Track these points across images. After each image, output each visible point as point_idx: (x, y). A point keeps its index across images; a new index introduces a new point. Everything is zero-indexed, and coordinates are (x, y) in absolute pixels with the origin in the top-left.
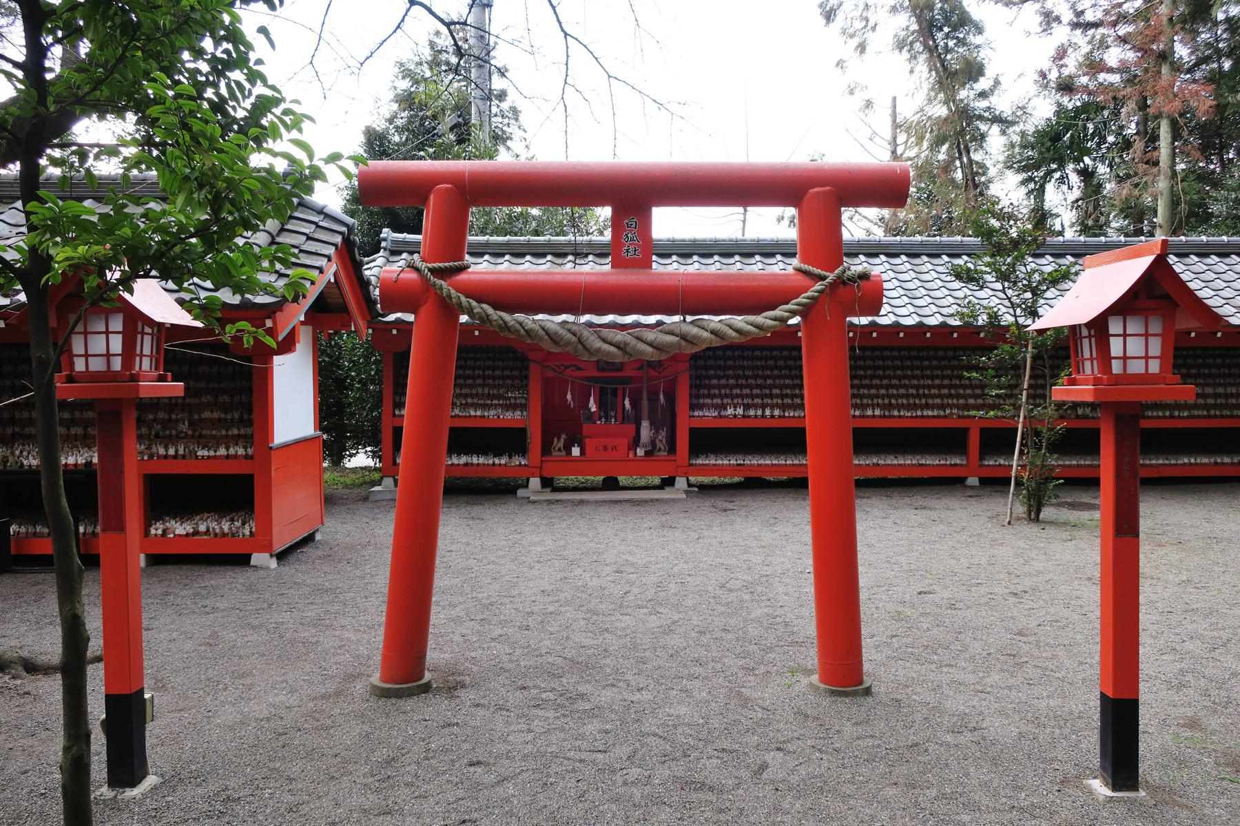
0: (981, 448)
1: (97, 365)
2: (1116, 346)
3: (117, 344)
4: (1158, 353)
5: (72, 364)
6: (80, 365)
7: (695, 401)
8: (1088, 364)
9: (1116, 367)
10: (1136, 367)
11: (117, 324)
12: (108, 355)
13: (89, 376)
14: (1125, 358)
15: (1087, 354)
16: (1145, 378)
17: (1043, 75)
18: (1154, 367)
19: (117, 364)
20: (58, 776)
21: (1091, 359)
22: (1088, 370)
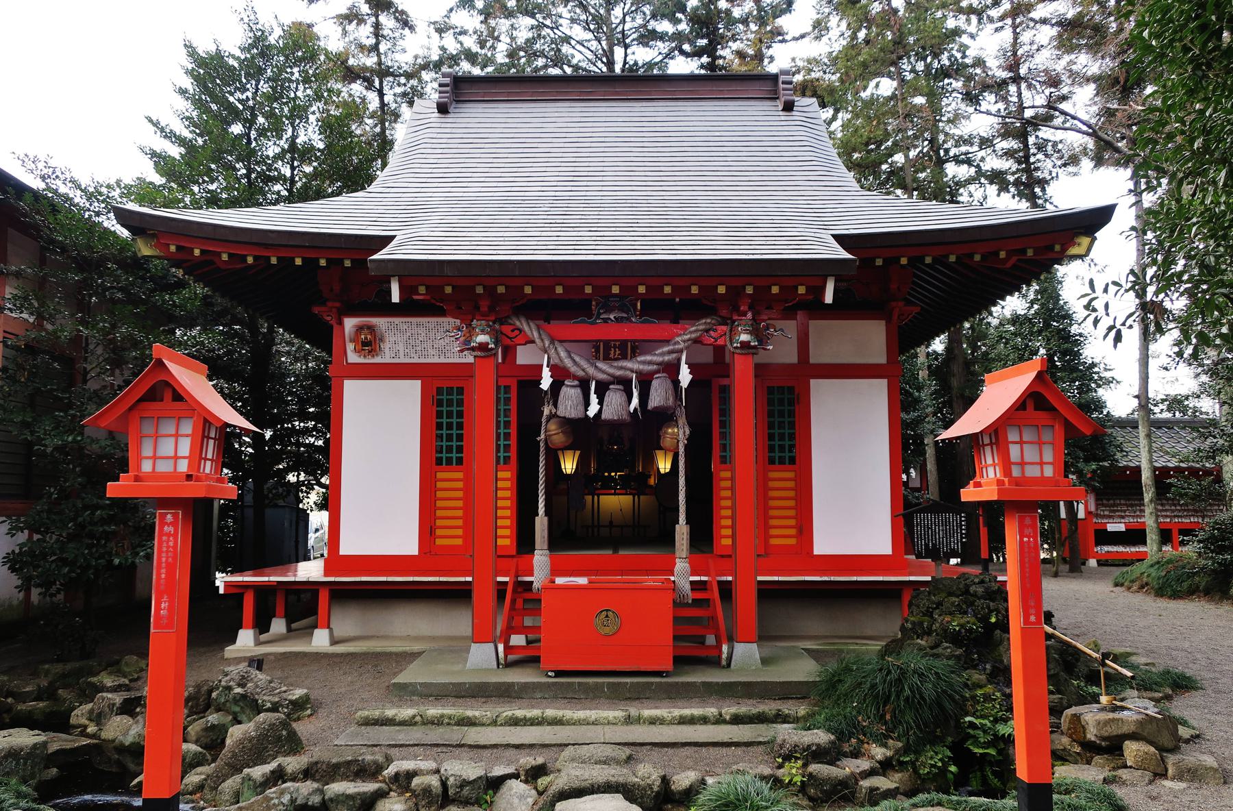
0: (190, 631)
1: (164, 467)
2: (1014, 452)
3: (185, 447)
4: (1051, 460)
5: (139, 467)
6: (147, 467)
7: (724, 663)
8: (991, 470)
9: (1016, 472)
10: (1032, 472)
11: (187, 427)
12: (176, 458)
13: (154, 475)
14: (1022, 464)
15: (989, 461)
16: (1042, 480)
17: (997, 30)
18: (1049, 471)
19: (183, 466)
20: (757, 541)
21: (994, 465)
22: (991, 475)
